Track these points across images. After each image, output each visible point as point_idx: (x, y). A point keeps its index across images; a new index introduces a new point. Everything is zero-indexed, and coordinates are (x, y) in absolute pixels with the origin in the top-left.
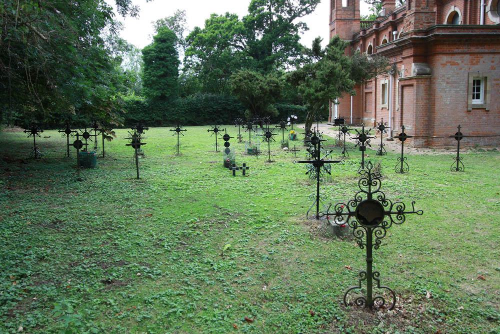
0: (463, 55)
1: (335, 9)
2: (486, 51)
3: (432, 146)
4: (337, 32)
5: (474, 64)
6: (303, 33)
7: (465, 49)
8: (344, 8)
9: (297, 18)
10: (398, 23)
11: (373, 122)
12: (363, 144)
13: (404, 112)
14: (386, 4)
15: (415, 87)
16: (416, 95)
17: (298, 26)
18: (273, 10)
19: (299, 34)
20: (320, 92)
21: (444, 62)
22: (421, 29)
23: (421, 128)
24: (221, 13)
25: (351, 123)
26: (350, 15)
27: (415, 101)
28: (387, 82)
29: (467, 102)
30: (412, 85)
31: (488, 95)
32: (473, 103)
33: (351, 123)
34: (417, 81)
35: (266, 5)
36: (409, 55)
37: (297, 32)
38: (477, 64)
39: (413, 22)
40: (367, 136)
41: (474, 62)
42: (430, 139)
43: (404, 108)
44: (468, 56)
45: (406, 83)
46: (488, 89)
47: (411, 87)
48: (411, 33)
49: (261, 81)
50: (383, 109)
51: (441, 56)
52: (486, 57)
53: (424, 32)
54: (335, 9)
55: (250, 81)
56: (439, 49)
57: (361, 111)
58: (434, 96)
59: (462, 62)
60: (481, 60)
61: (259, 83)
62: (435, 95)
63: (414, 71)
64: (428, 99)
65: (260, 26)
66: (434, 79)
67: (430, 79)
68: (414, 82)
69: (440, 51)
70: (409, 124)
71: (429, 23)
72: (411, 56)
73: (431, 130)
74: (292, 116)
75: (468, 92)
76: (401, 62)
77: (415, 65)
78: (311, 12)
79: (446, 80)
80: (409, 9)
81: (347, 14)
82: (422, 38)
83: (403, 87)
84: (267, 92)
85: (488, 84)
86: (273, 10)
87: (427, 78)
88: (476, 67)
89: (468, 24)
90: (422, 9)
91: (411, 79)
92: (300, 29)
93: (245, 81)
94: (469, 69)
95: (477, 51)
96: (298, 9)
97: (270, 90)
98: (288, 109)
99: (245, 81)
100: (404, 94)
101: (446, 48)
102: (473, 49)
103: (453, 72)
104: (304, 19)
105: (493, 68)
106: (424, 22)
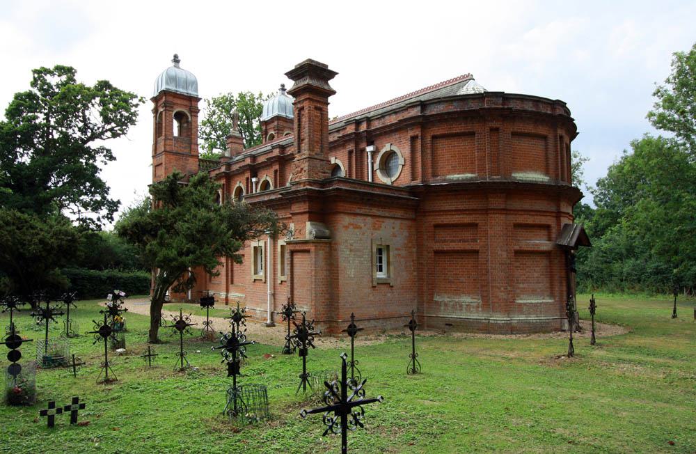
0: (365, 217)
1: (163, 137)
2: (387, 215)
3: (336, 333)
4: (165, 169)
5: (376, 229)
6: (106, 164)
7: (365, 210)
8: (175, 137)
9: (97, 141)
10: (259, 168)
11: (224, 297)
12: (304, 346)
13: (295, 286)
14: (231, 142)
15: (313, 255)
16: (315, 264)
17: (97, 152)
18: (52, 121)
19: (98, 164)
20: (187, 255)
21: (346, 224)
22: (316, 179)
23: (321, 308)
24: (7, 106)
25: (190, 298)
26: (185, 148)
27: (313, 273)
28: (262, 244)
29: (372, 276)
30: (308, 251)
31: (392, 268)
32: (378, 277)
33: (190, 298)
34: (315, 246)
35: (41, 113)
36: (303, 211)
37: (95, 161)
38: (379, 230)
39: (306, 168)
40: (310, 331)
41: (377, 226)
42: (334, 324)
43: (295, 281)
44: (369, 218)
45: (298, 247)
46: (391, 260)
47: (306, 254)
48: (304, 183)
49: (41, 230)
50: (283, 283)
51: (342, 215)
52: (389, 222)
53: (320, 184)
54: (163, 137)
55: (18, 229)
56: (342, 206)
57: (204, 281)
58: (338, 267)
59: (365, 225)
60: (383, 225)
61: (38, 234)
62: (338, 265)
63: (311, 233)
64: (329, 270)
65: (27, 142)
66: (336, 244)
67: (330, 243)
68: (312, 248)
69: (341, 209)
70: (304, 304)
71: (324, 173)
72: (304, 213)
73: (333, 311)
74: (116, 292)
75: (372, 263)
76: (290, 218)
77: (311, 224)
78: (119, 135)
79: (349, 247)
80: (299, 152)
81: (180, 146)
82: (319, 190)
83: (292, 253)
84: (52, 248)
85: (391, 254)
86: (52, 121)
87: (326, 243)
88: (378, 232)
89: (354, 177)
90: (316, 154)
91: (306, 242)
92: (100, 158)
93: (9, 228)
94: (372, 234)
95: (378, 213)
96: (99, 128)
97: (58, 246)
98: (76, 275)
99: (9, 228)
100: (295, 262)
101: (347, 207)
102: (375, 211)
103: (356, 235)
104: (109, 143)
105: (394, 236)
106: (319, 171)
